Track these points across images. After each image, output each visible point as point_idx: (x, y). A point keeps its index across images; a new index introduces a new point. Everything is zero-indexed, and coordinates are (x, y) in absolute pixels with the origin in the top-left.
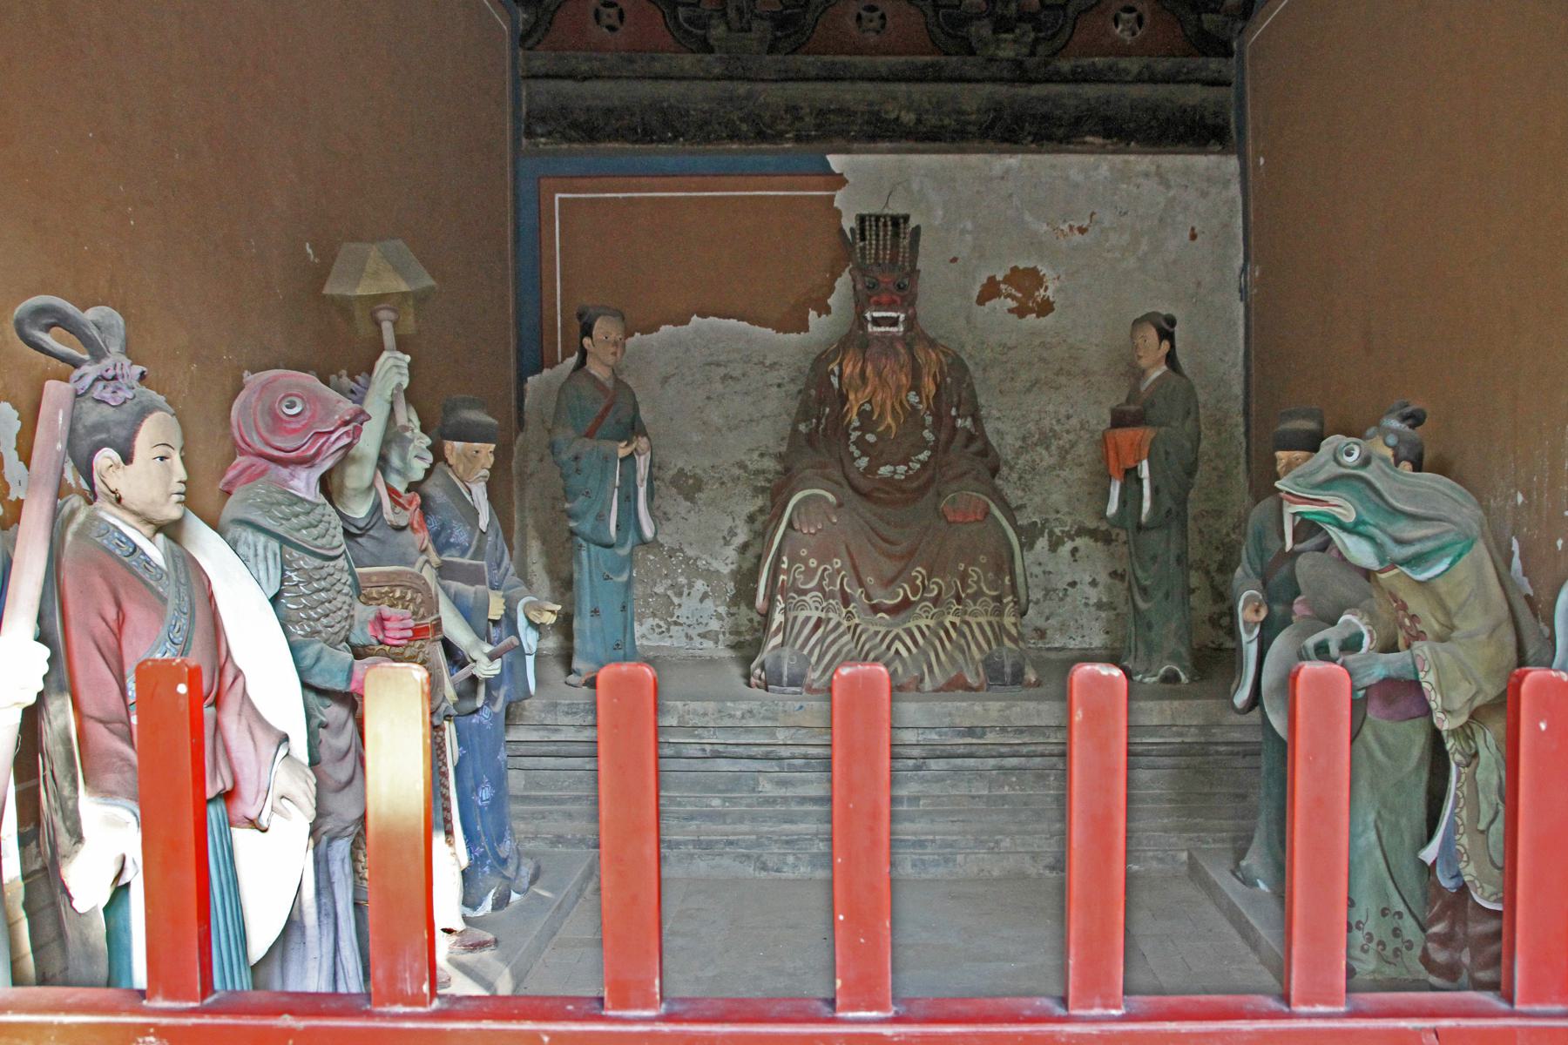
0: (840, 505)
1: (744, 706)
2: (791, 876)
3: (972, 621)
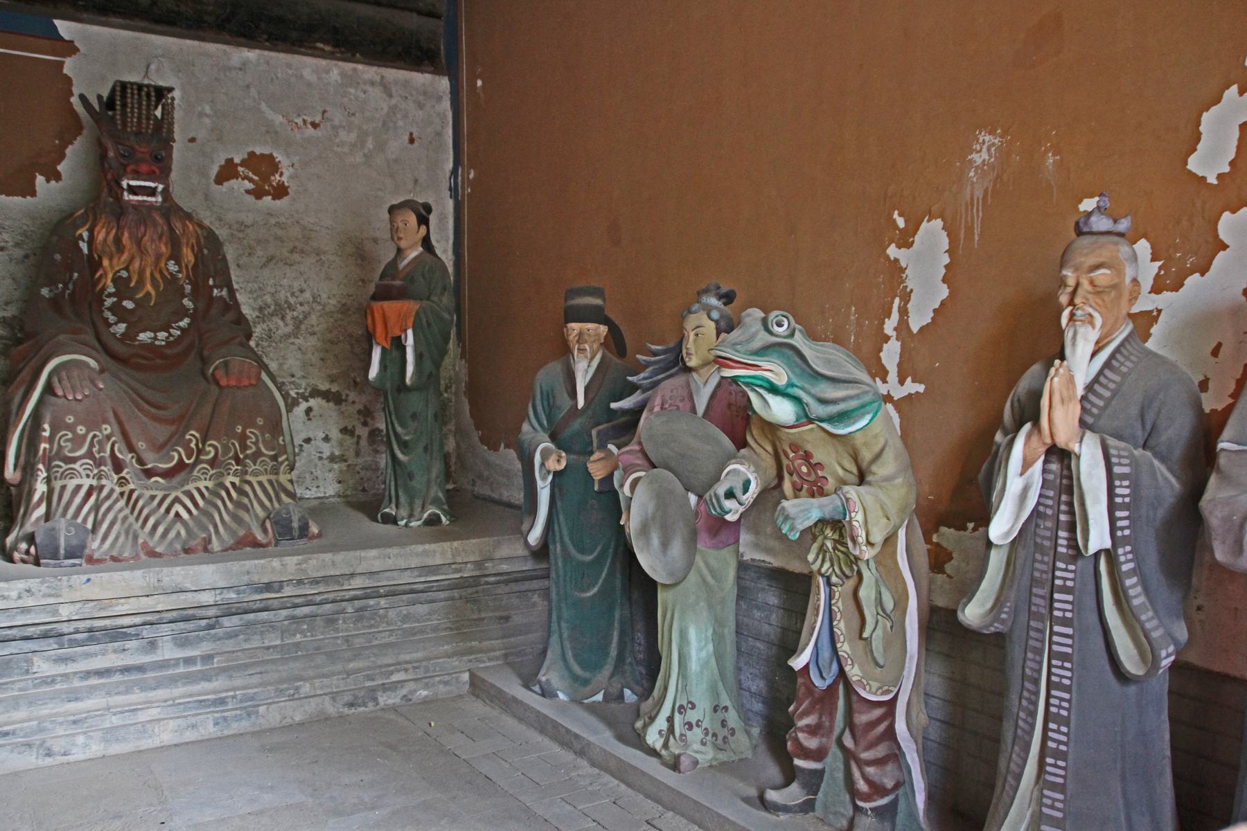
0: (102, 371)
1: (21, 585)
2: (81, 757)
3: (253, 479)
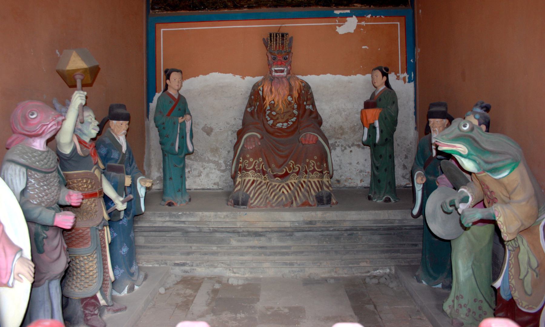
0: (262, 138)
3: (312, 180)
